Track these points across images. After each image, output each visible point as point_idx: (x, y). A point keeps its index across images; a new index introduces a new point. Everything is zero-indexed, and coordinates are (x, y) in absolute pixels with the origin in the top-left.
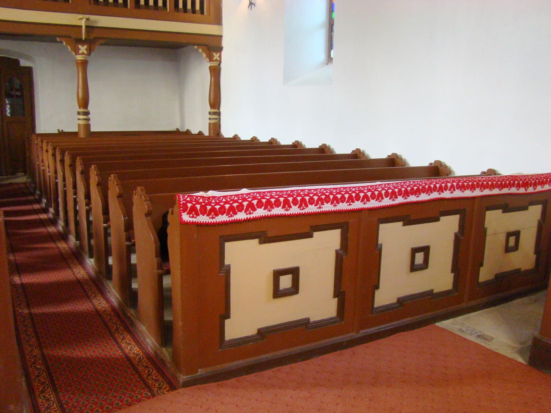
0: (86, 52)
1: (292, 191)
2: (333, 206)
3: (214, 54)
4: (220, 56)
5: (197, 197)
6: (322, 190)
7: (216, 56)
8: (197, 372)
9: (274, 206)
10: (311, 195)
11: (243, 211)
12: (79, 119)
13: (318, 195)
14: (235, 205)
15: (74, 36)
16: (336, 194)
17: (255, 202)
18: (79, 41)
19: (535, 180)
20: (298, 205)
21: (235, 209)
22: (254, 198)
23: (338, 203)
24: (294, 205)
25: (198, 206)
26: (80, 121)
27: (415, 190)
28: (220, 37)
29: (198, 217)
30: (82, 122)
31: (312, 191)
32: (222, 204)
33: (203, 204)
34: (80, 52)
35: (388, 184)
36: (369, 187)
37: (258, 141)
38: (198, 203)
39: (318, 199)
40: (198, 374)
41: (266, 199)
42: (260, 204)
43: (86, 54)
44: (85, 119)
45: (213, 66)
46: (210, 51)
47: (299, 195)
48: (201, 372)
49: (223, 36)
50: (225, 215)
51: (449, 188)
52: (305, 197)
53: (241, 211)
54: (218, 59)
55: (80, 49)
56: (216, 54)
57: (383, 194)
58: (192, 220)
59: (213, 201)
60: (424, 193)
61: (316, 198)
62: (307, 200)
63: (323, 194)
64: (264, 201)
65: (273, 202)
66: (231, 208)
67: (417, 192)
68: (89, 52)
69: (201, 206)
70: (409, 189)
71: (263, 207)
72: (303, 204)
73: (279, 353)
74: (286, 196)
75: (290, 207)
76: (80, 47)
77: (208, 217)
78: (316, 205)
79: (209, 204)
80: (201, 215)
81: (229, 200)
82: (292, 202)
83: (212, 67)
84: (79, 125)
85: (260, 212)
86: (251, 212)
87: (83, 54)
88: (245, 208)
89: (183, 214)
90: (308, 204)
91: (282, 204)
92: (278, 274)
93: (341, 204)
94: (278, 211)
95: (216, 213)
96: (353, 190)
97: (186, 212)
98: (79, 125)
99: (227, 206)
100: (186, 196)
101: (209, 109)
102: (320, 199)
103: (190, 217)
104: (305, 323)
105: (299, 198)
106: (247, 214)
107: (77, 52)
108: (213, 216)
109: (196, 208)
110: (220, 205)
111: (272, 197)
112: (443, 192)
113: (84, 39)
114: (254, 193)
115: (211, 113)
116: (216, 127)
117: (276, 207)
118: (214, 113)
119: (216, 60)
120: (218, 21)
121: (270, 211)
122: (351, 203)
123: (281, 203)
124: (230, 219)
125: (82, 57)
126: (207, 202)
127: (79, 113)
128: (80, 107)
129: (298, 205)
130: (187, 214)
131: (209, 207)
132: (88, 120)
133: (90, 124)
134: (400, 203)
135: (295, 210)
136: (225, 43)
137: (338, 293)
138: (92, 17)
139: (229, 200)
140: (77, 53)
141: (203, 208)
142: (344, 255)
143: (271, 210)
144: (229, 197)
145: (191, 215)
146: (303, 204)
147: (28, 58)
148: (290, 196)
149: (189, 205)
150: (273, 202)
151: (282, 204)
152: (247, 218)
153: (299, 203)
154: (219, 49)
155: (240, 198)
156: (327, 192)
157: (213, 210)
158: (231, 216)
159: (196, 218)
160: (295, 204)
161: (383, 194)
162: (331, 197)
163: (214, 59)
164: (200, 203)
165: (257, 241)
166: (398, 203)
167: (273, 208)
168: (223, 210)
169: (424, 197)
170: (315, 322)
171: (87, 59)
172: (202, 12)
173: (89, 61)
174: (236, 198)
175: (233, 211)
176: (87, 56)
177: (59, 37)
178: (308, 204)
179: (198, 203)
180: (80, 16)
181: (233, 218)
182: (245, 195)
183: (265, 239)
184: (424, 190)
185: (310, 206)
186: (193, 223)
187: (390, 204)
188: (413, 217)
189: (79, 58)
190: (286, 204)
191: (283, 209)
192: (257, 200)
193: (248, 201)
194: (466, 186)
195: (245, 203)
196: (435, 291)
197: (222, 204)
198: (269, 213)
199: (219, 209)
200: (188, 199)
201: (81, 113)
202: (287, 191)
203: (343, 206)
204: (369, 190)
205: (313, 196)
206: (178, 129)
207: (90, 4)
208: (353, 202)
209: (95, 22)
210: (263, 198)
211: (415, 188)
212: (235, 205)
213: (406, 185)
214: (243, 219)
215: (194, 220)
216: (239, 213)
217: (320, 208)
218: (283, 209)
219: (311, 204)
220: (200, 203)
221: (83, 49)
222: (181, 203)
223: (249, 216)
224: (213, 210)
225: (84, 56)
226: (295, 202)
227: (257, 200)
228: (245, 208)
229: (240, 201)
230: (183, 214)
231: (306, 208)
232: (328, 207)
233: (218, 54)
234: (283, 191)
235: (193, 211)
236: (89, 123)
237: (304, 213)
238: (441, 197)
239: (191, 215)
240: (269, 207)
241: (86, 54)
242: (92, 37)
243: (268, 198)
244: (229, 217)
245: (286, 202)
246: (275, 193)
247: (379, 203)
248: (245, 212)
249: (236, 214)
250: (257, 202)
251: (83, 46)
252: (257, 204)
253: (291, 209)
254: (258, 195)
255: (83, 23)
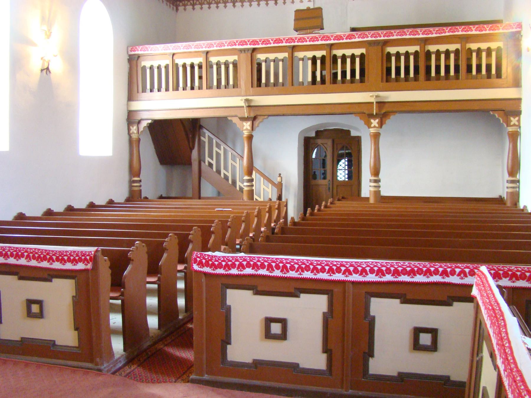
0: (377, 125)
1: (277, 259)
2: (314, 274)
3: (512, 119)
4: (519, 121)
5: (205, 255)
6: (274, 259)
7: (514, 121)
8: (203, 375)
9: (401, 274)
10: (292, 264)
11: (236, 268)
12: (370, 186)
13: (298, 264)
14: (230, 263)
15: (367, 112)
16: (316, 265)
17: (245, 263)
18: (371, 116)
19: (79, 257)
20: (280, 270)
21: (229, 267)
22: (245, 260)
23: (77, 263)
24: (276, 269)
25: (204, 261)
26: (371, 187)
27: (408, 270)
28: (519, 100)
29: (204, 268)
30: (372, 189)
31: (324, 262)
32: (220, 261)
33: (207, 260)
34: (372, 126)
35: (376, 262)
36: (353, 263)
37: (24, 216)
38: (204, 258)
39: (298, 267)
40: (204, 377)
41: (253, 262)
42: (248, 265)
43: (377, 127)
44: (375, 186)
45: (511, 131)
46: (507, 116)
47: (282, 262)
48: (206, 377)
49: (522, 99)
50: (222, 269)
51: (440, 273)
52: (287, 265)
53: (234, 268)
54: (517, 123)
55: (372, 123)
56: (514, 118)
57: (368, 270)
58: (200, 269)
59: (214, 259)
60: (420, 274)
61: (296, 266)
62: (289, 267)
63: (304, 264)
64: (252, 263)
65: (259, 265)
66: (227, 265)
67: (412, 273)
68: (380, 125)
69: (206, 261)
70: (400, 269)
71: (251, 268)
72: (285, 270)
73: (268, 384)
74: (270, 262)
75: (31, 260)
76: (372, 121)
77: (210, 269)
78: (296, 272)
79: (211, 260)
80: (205, 267)
81: (225, 259)
82: (275, 267)
83: (509, 133)
84: (370, 191)
85: (249, 271)
86: (242, 270)
87: (375, 127)
88: (237, 266)
89: (194, 264)
90: (289, 270)
91: (266, 267)
92: (417, 331)
93: (321, 274)
94: (263, 272)
95: (216, 267)
96: (335, 263)
97: (196, 264)
98: (370, 191)
99: (224, 263)
100: (199, 254)
101: (507, 177)
102: (300, 267)
103: (199, 267)
104: (294, 367)
105: (281, 265)
106: (239, 271)
107: (369, 125)
108: (300, 273)
109: (203, 262)
110: (291, 264)
111: (259, 261)
112: (448, 276)
113: (375, 114)
114: (246, 257)
115: (509, 182)
116: (515, 196)
117: (261, 269)
118: (512, 182)
119: (514, 125)
120: (517, 83)
121: (315, 274)
122: (332, 274)
123: (265, 266)
124: (226, 272)
125: (374, 130)
126: (210, 258)
127: (370, 181)
128: (372, 175)
129: (280, 270)
130: (197, 265)
131: (210, 263)
132: (379, 187)
133: (380, 191)
134: (389, 280)
135: (277, 273)
136: (524, 107)
137: (326, 349)
138: (381, 94)
139: (225, 259)
140: (369, 127)
141: (207, 262)
142: (330, 318)
143: (258, 271)
144: (226, 257)
145: (199, 266)
146: (285, 270)
147: (356, 129)
148: (274, 262)
149: (198, 259)
150: (259, 265)
151: (266, 267)
152: (239, 274)
153: (281, 268)
154: (518, 113)
155: (234, 259)
156: (308, 263)
157: (213, 264)
158: (227, 271)
159: (202, 268)
160: (278, 269)
161: (368, 270)
162: (311, 267)
163: (512, 123)
164: (205, 259)
165: (16, 277)
166: (387, 280)
167: (259, 269)
168: (45, 258)
169: (419, 278)
170: (303, 369)
171: (380, 132)
172: (499, 75)
173: (381, 133)
174: (231, 259)
175: (228, 267)
176: (380, 129)
177: (491, 111)
178: (289, 270)
179: (204, 258)
180: (371, 94)
181: (228, 272)
182: (238, 257)
183: (405, 301)
184: (420, 272)
185: (291, 272)
186: (200, 272)
187: (377, 280)
188: (408, 297)
189: (372, 130)
190: (270, 268)
191: (268, 272)
192: (246, 262)
193: (239, 262)
194: (433, 272)
195: (237, 263)
196: (228, 346)
197: (220, 261)
198: (395, 280)
199: (218, 264)
200: (199, 256)
201: (373, 181)
202: (272, 258)
203: (324, 276)
204: (351, 265)
205: (294, 264)
206: (500, 196)
207: (382, 81)
208: (334, 273)
209: (387, 97)
210: (251, 261)
211: (408, 269)
212: (230, 263)
213: (241, 260)
214: (236, 274)
215: (201, 269)
216: (232, 269)
217: (300, 274)
218: (343, 276)
219: (292, 270)
220: (205, 259)
221: (375, 122)
222: (194, 257)
223: (240, 272)
224: (74, 259)
225: (375, 129)
226: (278, 267)
227: (246, 262)
228: (237, 266)
229: (233, 261)
230: (194, 264)
231: (288, 273)
232: (308, 275)
233: (517, 118)
234: (269, 258)
235: (200, 264)
236: (380, 190)
237: (273, 275)
238: (445, 281)
239: (345, 275)
240: (256, 268)
241: (377, 127)
242: (383, 111)
243: (255, 261)
244: (225, 271)
245: (28, 256)
246: (262, 258)
247: (363, 278)
248: (237, 269)
249: (230, 269)
250: (247, 263)
251: (375, 120)
252: (246, 265)
253: (274, 272)
254: (248, 259)
255: (373, 100)
